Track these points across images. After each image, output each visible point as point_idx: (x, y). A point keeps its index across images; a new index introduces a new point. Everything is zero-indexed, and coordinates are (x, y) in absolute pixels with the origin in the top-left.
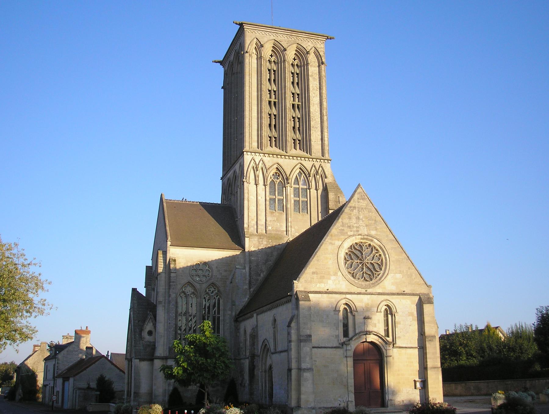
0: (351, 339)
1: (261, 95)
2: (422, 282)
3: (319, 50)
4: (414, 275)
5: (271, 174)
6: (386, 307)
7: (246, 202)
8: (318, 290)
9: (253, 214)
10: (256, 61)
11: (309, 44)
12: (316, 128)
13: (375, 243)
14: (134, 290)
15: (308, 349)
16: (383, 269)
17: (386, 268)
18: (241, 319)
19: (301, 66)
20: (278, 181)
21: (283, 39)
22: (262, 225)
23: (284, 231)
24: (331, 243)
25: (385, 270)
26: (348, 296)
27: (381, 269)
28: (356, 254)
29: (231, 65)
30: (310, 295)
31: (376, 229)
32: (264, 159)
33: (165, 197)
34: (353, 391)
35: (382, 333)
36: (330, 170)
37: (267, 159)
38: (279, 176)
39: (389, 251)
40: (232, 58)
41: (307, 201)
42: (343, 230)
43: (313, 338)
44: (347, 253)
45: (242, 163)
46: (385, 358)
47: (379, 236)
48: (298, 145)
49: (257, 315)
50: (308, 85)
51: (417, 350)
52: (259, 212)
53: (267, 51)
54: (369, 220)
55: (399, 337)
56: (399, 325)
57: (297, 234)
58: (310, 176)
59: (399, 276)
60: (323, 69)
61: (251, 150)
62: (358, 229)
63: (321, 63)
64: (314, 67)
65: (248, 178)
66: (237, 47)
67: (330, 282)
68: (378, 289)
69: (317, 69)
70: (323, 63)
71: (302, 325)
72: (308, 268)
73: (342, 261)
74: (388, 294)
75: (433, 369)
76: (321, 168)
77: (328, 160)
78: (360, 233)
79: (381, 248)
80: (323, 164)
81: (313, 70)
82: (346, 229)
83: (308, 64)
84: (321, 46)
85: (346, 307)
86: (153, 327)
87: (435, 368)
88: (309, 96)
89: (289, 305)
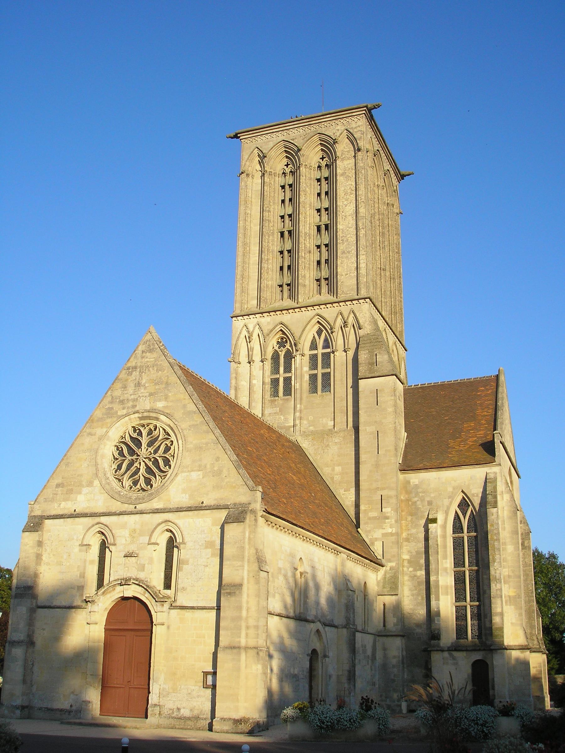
8: (61, 513)
11: (338, 127)
12: (349, 252)
13: (162, 422)
20: (284, 350)
21: (296, 134)
23: (290, 427)
24: (90, 434)
26: (103, 519)
31: (166, 398)
38: (286, 341)
42: (112, 408)
54: (156, 384)
55: (184, 589)
60: (360, 157)
61: (243, 313)
62: (135, 403)
64: (349, 159)
67: (80, 497)
68: (156, 504)
74: (170, 511)
75: (229, 651)
78: (137, 408)
81: (344, 165)
82: (116, 406)
87: (234, 648)
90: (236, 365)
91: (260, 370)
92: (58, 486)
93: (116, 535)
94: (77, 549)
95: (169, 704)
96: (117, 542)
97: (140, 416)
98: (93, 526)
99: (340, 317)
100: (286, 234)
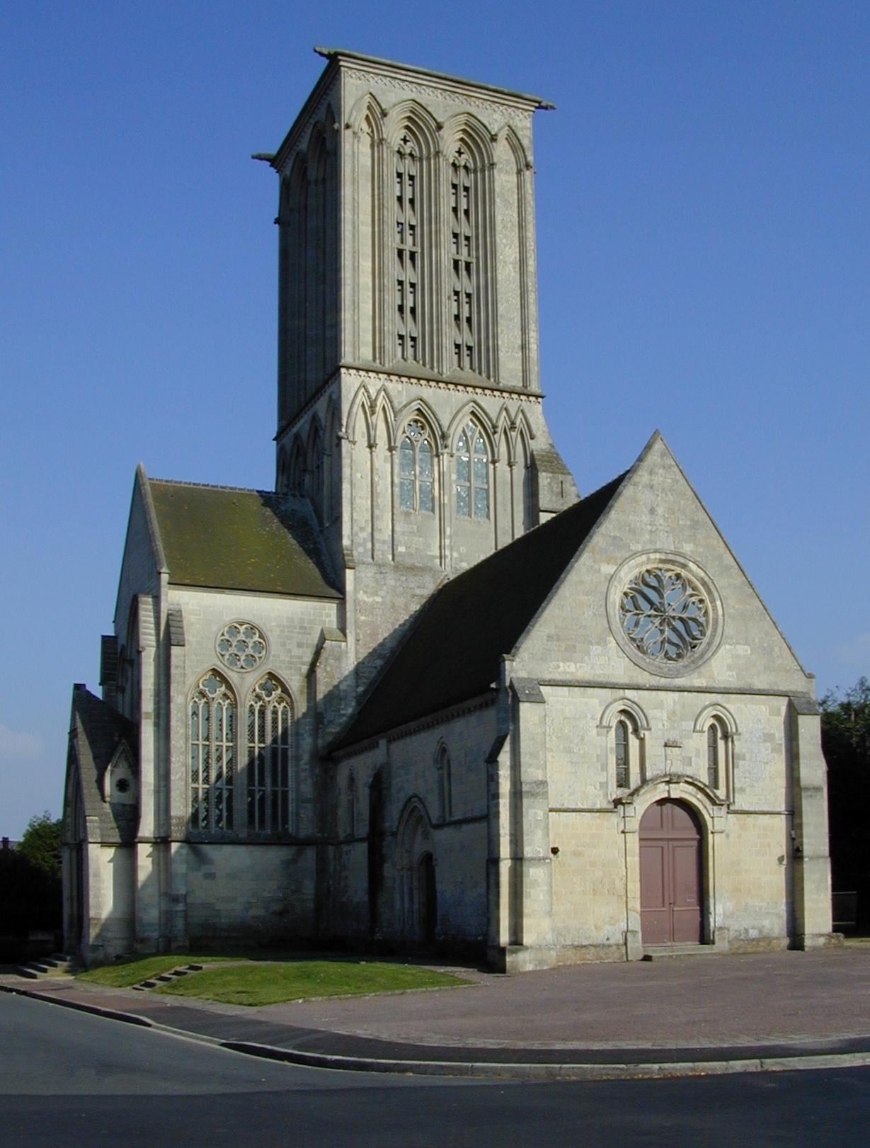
0: (637, 791)
1: (381, 233)
2: (795, 666)
3: (520, 134)
4: (776, 649)
5: (405, 423)
6: (712, 721)
7: (346, 487)
9: (363, 517)
10: (369, 151)
11: (496, 116)
13: (691, 571)
14: (79, 688)
15: (540, 815)
16: (708, 633)
17: (715, 630)
18: (341, 753)
19: (475, 172)
22: (384, 542)
23: (435, 557)
25: (713, 635)
26: (629, 694)
27: (703, 634)
28: (646, 595)
29: (302, 164)
30: (545, 690)
32: (390, 386)
33: (148, 473)
34: (638, 908)
35: (704, 778)
36: (542, 421)
37: (395, 386)
38: (423, 427)
39: (723, 593)
40: (303, 145)
41: (487, 491)
43: (551, 789)
44: (626, 594)
45: (334, 397)
46: (710, 836)
47: (702, 556)
48: (467, 360)
49: (389, 742)
50: (492, 217)
51: (783, 817)
52: (377, 512)
53: (394, 131)
55: (742, 790)
56: (741, 762)
57: (465, 566)
58: (495, 433)
59: (743, 650)
61: (357, 364)
63: (523, 167)
64: (507, 172)
65: (350, 431)
66: (321, 114)
69: (514, 178)
70: (528, 166)
71: (524, 759)
72: (537, 625)
73: (615, 611)
76: (521, 416)
77: (537, 397)
78: (658, 546)
79: (704, 584)
80: (525, 405)
83: (492, 165)
84: (524, 122)
85: (623, 718)
86: (129, 772)
88: (493, 244)
89: (491, 714)
90: (350, 445)
91: (385, 461)
92: (549, 637)
93: (649, 717)
94: (594, 731)
95: (735, 926)
96: (652, 723)
97: (663, 557)
98: (615, 701)
99: (504, 413)
100: (462, 266)
